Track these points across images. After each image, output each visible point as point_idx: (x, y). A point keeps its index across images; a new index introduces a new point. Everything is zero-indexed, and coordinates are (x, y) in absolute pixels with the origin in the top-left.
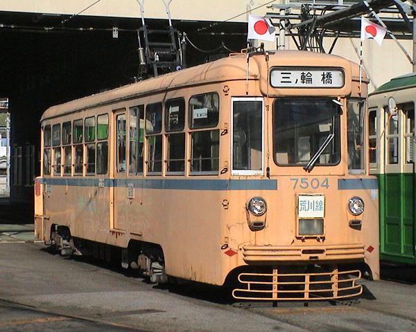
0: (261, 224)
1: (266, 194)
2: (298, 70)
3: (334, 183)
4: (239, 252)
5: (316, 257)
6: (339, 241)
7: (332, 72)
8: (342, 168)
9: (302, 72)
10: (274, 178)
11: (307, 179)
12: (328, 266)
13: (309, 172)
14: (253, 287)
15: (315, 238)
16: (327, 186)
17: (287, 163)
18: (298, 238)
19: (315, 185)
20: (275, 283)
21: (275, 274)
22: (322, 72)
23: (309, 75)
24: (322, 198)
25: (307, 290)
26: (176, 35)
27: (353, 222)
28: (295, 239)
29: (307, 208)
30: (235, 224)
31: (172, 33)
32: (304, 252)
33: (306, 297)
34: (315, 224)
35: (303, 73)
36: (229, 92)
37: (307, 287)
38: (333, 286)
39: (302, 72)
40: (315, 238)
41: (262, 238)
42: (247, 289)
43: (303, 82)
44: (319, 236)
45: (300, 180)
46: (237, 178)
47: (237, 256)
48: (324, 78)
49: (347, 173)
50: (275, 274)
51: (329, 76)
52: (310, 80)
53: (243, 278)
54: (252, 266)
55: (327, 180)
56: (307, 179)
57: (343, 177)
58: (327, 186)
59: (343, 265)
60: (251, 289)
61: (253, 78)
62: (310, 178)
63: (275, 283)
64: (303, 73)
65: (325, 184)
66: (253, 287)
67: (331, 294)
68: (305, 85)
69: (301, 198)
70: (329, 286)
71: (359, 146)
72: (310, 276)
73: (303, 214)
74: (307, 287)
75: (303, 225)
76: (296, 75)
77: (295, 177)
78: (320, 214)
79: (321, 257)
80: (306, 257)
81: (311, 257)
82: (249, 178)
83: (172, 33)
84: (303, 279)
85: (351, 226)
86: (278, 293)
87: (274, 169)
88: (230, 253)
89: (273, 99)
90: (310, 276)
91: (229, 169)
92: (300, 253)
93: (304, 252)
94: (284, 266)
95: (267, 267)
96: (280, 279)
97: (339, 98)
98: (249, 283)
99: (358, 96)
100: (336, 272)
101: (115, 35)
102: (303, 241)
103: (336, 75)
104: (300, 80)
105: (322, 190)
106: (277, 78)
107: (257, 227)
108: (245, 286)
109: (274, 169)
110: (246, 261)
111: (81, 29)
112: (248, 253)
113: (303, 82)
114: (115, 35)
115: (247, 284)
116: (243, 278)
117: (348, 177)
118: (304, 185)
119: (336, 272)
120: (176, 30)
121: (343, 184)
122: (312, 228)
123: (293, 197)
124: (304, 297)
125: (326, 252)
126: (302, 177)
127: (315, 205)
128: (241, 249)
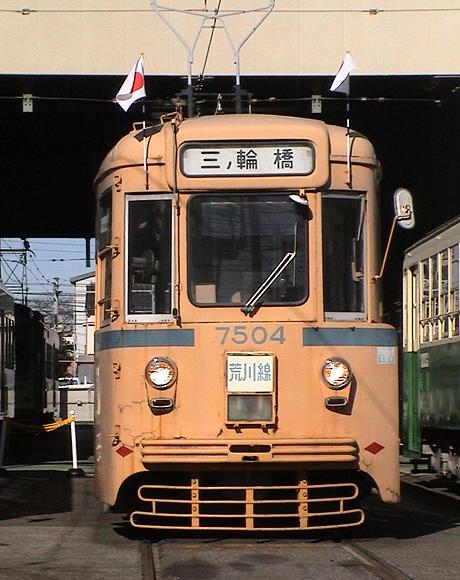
0: (167, 402)
1: (176, 353)
2: (231, 146)
3: (295, 334)
4: (135, 449)
5: (256, 458)
6: (303, 429)
7: (294, 149)
8: (312, 307)
9: (239, 150)
10: (189, 326)
11: (244, 328)
12: (287, 473)
13: (251, 317)
14: (161, 507)
15: (258, 426)
16: (282, 340)
17: (213, 300)
18: (229, 427)
19: (259, 338)
20: (195, 501)
21: (195, 486)
22: (274, 150)
23: (251, 154)
24: (270, 360)
25: (250, 512)
26: (244, 98)
27: (332, 401)
28: (225, 429)
29: (242, 376)
30: (129, 403)
31: (238, 98)
32: (234, 449)
33: (250, 526)
34: (261, 403)
35: (241, 152)
36: (122, 187)
37: (250, 509)
38: (300, 508)
39: (239, 150)
40: (258, 426)
41: (170, 427)
42: (152, 511)
43: (241, 167)
44: (264, 423)
45: (232, 329)
46: (131, 327)
47: (132, 457)
48: (278, 159)
49: (320, 318)
50: (195, 486)
51: (288, 155)
52: (253, 163)
53: (145, 493)
54: (157, 473)
55: (281, 329)
56: (244, 328)
57: (315, 325)
58: (282, 340)
59: (316, 472)
60: (157, 512)
61: (156, 162)
62: (250, 327)
63: (195, 501)
64: (241, 152)
65: (278, 336)
66: (161, 507)
67: (296, 522)
68: (244, 171)
69: (231, 360)
70: (294, 508)
71: (359, 274)
72: (255, 491)
73: (235, 386)
74: (250, 509)
75: (239, 404)
76: (228, 155)
77: (227, 325)
78: (267, 386)
79: (263, 457)
80: (237, 457)
81: (245, 458)
82: (150, 327)
83: (238, 98)
84: (242, 495)
85: (327, 407)
86: (201, 518)
87: (187, 311)
88: (124, 451)
89: (189, 195)
90: (255, 491)
91: (121, 313)
92: (226, 450)
93: (234, 449)
94: (210, 473)
95: (178, 473)
96: (203, 495)
97: (302, 192)
98: (154, 501)
99: (348, 188)
100: (303, 486)
101: (28, 108)
102: (238, 432)
103: (299, 153)
104: (235, 164)
105: (272, 346)
106: (195, 161)
107: (161, 408)
108: (347, 505)
109: (187, 311)
110: (146, 464)
111: (364, 99)
112: (148, 450)
113: (241, 167)
114: (28, 108)
115: (151, 503)
116: (145, 493)
117: (321, 324)
118: (240, 338)
119: (303, 486)
120: (244, 92)
121: (314, 335)
122: (249, 409)
123: (221, 358)
124: (244, 526)
125: (272, 451)
126: (238, 325)
127: (257, 369)
128: (137, 445)
